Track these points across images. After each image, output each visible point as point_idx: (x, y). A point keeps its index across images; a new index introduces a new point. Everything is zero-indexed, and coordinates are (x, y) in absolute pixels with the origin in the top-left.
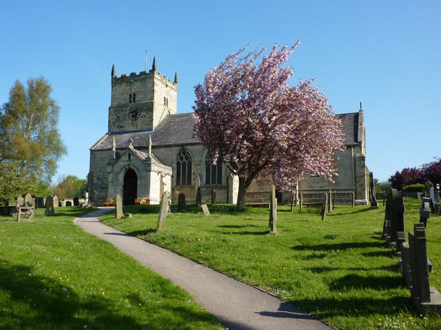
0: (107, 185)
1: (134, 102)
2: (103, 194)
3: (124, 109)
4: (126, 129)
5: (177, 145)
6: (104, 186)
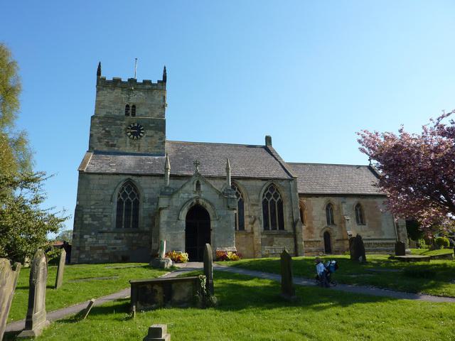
1: (134, 114)
2: (101, 242)
3: (119, 122)
4: (121, 149)
5: (263, 179)
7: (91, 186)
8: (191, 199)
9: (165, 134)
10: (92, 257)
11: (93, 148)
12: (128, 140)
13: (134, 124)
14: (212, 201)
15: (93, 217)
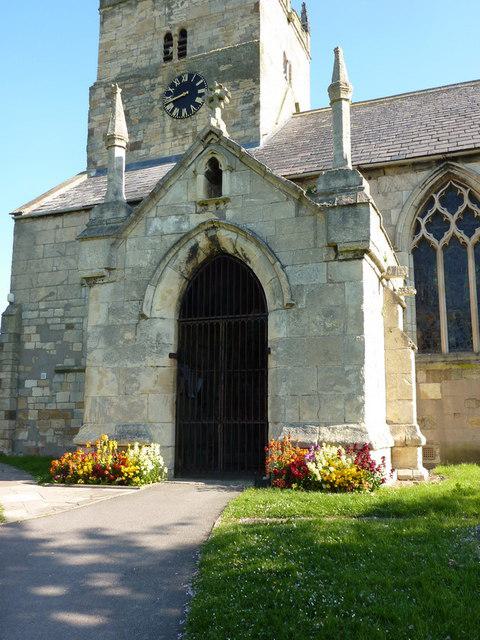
0: (82, 355)
1: (182, 54)
2: (61, 396)
3: (147, 82)
4: (154, 152)
5: (416, 165)
6: (69, 362)
7: (39, 250)
8: (187, 236)
9: (258, 83)
10: (44, 438)
11: (95, 163)
12: (169, 121)
13: (180, 78)
14: (266, 230)
15: (44, 330)
